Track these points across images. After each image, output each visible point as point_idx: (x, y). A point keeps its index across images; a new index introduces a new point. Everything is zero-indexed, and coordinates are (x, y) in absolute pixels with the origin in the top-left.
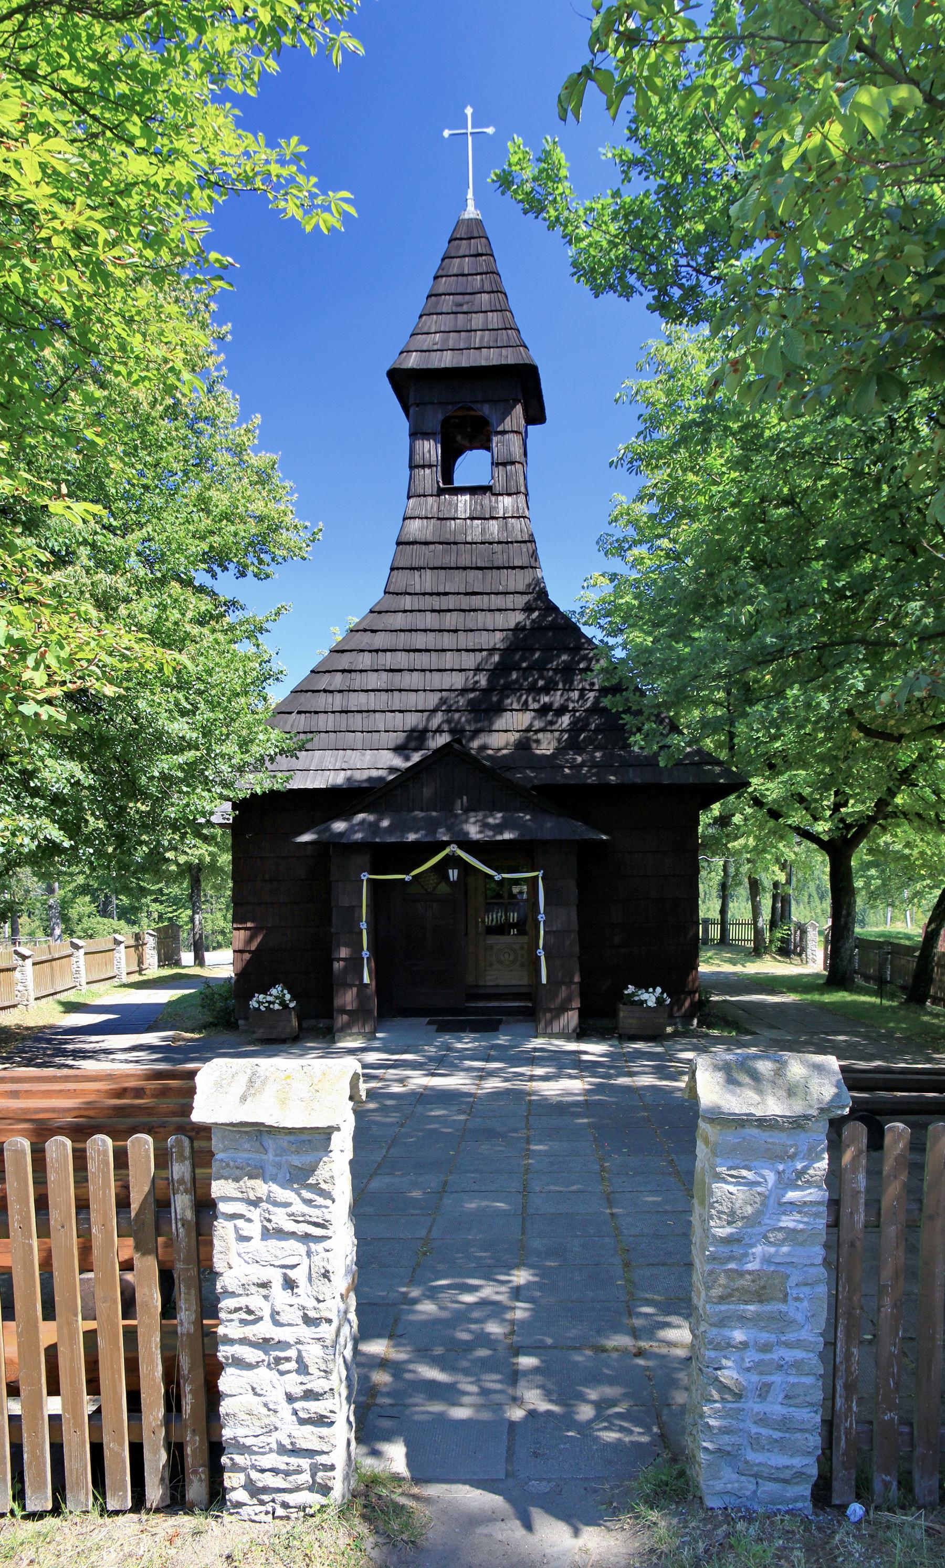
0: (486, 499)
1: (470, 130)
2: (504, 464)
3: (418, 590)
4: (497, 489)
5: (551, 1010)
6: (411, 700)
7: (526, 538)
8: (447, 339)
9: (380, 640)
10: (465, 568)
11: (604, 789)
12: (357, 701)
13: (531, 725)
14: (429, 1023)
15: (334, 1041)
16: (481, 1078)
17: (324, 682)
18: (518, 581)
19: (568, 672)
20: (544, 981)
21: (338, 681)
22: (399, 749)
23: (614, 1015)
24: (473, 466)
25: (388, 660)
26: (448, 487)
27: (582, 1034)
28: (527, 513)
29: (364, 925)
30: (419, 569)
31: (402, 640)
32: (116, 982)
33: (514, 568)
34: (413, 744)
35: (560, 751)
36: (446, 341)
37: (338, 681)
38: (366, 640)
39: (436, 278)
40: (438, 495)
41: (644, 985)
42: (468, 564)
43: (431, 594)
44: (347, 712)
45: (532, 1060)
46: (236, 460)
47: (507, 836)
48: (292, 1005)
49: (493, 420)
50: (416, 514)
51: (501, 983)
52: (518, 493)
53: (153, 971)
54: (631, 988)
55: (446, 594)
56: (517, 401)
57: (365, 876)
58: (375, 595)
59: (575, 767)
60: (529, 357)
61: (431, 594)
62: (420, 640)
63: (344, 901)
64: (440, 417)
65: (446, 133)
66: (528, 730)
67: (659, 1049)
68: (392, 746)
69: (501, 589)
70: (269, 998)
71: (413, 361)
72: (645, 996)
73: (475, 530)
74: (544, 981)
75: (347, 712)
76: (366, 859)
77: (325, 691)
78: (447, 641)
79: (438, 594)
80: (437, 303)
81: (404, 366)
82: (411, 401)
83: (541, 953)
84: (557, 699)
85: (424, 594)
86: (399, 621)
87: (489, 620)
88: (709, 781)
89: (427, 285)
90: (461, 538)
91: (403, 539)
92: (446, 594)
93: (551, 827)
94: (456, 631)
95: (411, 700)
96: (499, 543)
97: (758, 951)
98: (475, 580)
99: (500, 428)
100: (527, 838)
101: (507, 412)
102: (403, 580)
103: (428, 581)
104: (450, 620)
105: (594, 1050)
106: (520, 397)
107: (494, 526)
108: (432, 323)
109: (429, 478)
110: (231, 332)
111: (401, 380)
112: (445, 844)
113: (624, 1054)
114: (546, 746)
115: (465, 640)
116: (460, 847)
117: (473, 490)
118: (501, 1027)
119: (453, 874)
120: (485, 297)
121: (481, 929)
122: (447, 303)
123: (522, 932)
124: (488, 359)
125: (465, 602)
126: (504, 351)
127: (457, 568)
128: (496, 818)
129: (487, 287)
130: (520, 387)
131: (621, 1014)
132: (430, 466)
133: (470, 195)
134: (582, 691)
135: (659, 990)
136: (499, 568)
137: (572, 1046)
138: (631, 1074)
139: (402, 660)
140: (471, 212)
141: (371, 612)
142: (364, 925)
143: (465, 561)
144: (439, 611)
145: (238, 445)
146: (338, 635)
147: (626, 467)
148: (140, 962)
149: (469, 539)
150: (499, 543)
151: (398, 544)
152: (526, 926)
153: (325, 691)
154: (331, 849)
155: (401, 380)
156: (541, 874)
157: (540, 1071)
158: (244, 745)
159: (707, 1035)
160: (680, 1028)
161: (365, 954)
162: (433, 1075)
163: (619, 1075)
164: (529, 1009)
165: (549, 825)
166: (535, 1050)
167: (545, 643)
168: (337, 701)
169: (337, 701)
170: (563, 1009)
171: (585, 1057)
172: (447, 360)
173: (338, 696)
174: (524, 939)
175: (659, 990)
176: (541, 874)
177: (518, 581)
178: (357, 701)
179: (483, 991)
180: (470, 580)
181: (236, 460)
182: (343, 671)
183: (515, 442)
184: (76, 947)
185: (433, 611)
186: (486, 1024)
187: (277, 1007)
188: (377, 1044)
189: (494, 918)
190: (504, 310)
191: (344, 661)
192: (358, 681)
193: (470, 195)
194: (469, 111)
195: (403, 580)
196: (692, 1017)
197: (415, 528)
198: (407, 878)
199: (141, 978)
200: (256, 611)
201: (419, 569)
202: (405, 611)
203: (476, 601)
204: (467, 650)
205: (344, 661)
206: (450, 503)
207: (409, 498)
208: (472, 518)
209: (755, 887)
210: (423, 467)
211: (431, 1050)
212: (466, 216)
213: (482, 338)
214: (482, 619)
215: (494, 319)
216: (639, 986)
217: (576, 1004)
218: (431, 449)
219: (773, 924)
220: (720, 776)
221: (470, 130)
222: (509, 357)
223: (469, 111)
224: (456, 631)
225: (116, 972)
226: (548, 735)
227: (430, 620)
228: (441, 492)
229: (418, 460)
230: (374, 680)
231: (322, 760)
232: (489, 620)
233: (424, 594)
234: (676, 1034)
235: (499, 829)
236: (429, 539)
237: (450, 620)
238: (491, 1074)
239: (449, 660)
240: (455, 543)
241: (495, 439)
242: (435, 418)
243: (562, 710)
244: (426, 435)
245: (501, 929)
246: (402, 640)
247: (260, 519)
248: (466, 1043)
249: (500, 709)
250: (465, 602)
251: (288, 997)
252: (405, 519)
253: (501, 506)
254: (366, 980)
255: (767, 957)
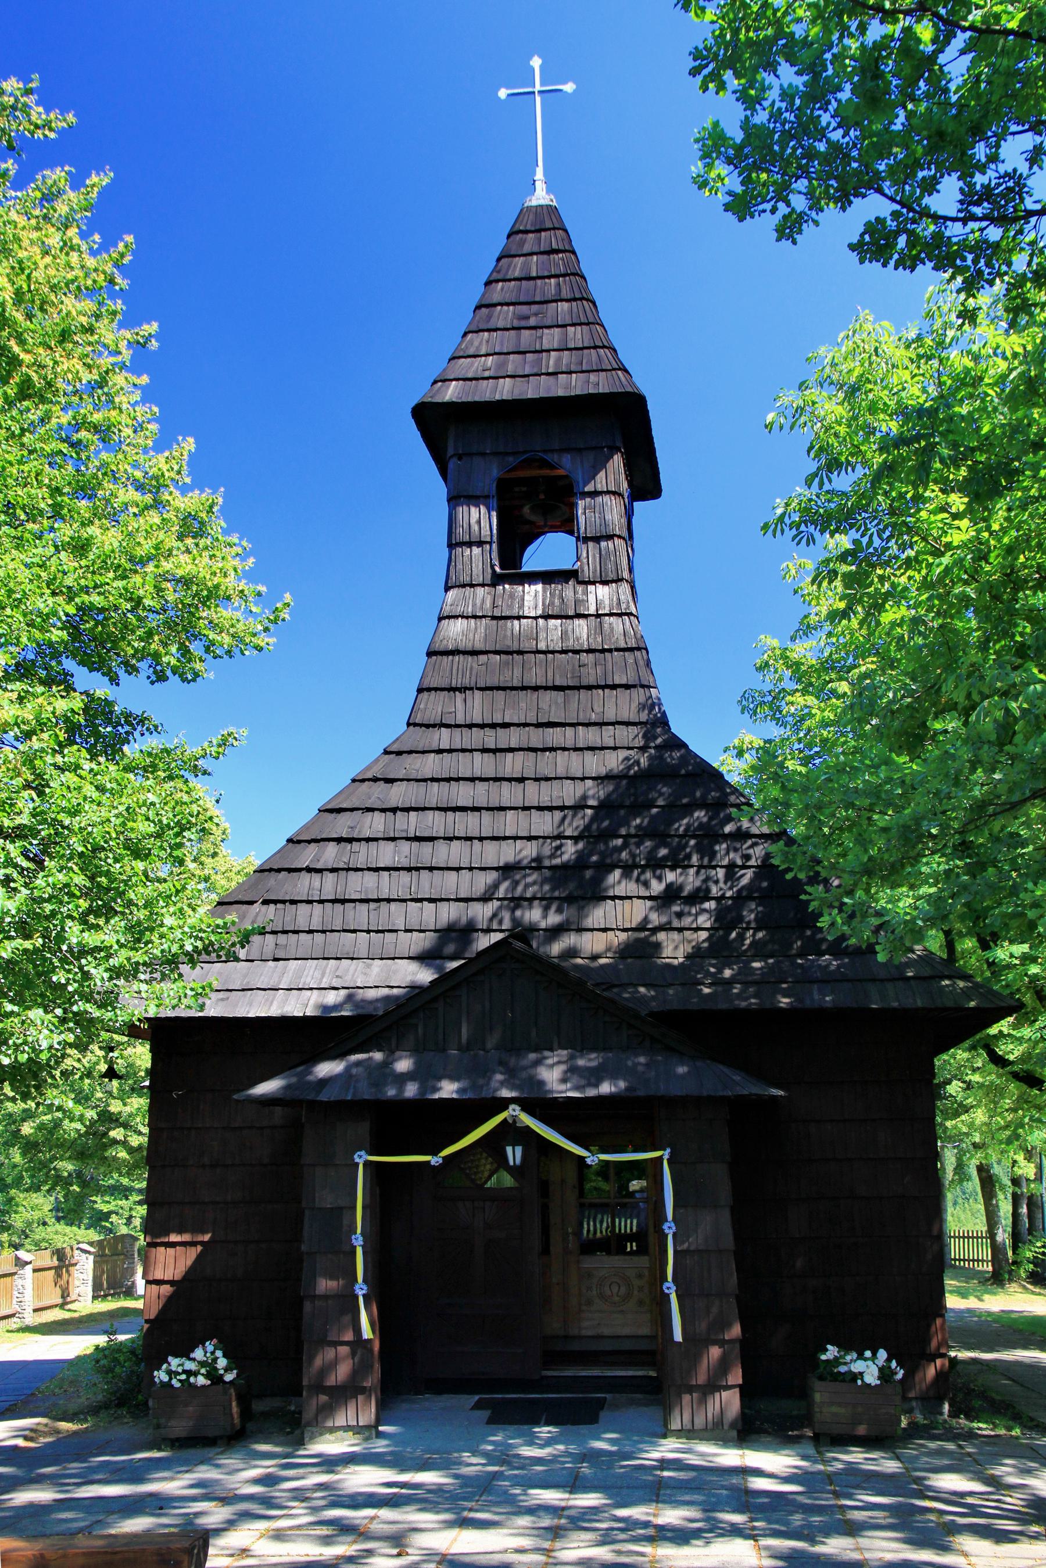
0: (569, 590)
1: (538, 87)
2: (597, 539)
3: (460, 720)
4: (586, 574)
5: (690, 1389)
6: (450, 883)
7: (632, 643)
8: (504, 364)
9: (397, 794)
10: (536, 688)
11: (770, 1017)
12: (359, 885)
13: (646, 920)
14: (478, 1406)
15: (301, 1443)
16: (555, 1533)
17: (307, 856)
18: (624, 705)
19: (708, 838)
20: (678, 1336)
21: (330, 855)
22: (424, 958)
23: (804, 1394)
24: (549, 551)
25: (412, 823)
26: (510, 570)
27: (746, 1431)
28: (634, 611)
29: (358, 1240)
30: (463, 689)
31: (435, 794)
32: (14, 1323)
33: (614, 687)
34: (450, 949)
35: (696, 955)
36: (502, 365)
37: (330, 855)
38: (376, 794)
39: (488, 284)
40: (494, 585)
41: (858, 1345)
42: (541, 682)
43: (482, 726)
44: (343, 901)
45: (656, 1488)
46: (148, 499)
47: (606, 1088)
48: (229, 1377)
49: (579, 476)
50: (459, 610)
51: (607, 1332)
52: (618, 580)
53: (85, 1304)
54: (832, 1352)
55: (506, 725)
56: (614, 449)
57: (361, 1158)
58: (393, 728)
59: (718, 982)
60: (632, 384)
61: (482, 726)
62: (463, 794)
63: (326, 1199)
64: (495, 472)
65: (503, 93)
66: (641, 927)
67: (891, 1466)
68: (414, 950)
69: (594, 718)
70: (190, 1366)
71: (451, 393)
72: (858, 1366)
73: (553, 632)
74: (678, 1336)
75: (343, 901)
76: (363, 1129)
77: (309, 870)
78: (508, 794)
79: (493, 726)
80: (489, 317)
81: (438, 399)
82: (450, 451)
83: (670, 1288)
84: (691, 880)
85: (470, 726)
86: (430, 765)
87: (574, 764)
88: (950, 1004)
89: (476, 292)
90: (526, 646)
91: (438, 646)
92: (506, 725)
93: (682, 1074)
94: (521, 780)
95: (450, 883)
96: (590, 651)
97: (998, 1278)
98: (552, 706)
99: (589, 488)
100: (641, 1093)
101: (600, 465)
102: (435, 707)
103: (477, 707)
104: (513, 764)
105: (773, 1465)
106: (619, 444)
107: (581, 629)
108: (480, 342)
109: (478, 561)
110: (157, 336)
111: (434, 421)
112: (503, 1104)
113: (829, 1478)
114: (674, 949)
115: (533, 794)
116: (523, 1109)
117: (548, 577)
118: (603, 1414)
119: (514, 1154)
120: (564, 306)
121: (572, 1244)
122: (505, 316)
123: (643, 1250)
124: (568, 386)
125: (536, 737)
126: (593, 377)
127: (524, 688)
128: (587, 1061)
129: (566, 293)
130: (620, 424)
131: (817, 1397)
132: (480, 544)
133: (539, 174)
134: (731, 868)
135: (882, 1354)
136: (589, 688)
137: (730, 1457)
138: (852, 1529)
139: (434, 823)
140: (541, 196)
141: (386, 752)
142: (358, 1240)
143: (535, 677)
144: (494, 751)
145: (156, 478)
146: (330, 785)
147: (790, 534)
148: (65, 1294)
149: (542, 646)
150: (590, 651)
151: (430, 654)
152: (648, 1241)
153: (309, 870)
154: (305, 1109)
155: (434, 421)
156: (666, 1154)
157: (671, 1516)
158: (137, 934)
159: (970, 1435)
160: (919, 1418)
161: (361, 1289)
162: (464, 1523)
163: (828, 1531)
164: (650, 1383)
165: (681, 1070)
166: (664, 1464)
167: (663, 797)
168: (329, 885)
169: (329, 885)
170: (713, 1386)
171: (759, 1484)
172: (505, 390)
173: (330, 877)
174: (643, 1261)
175: (882, 1354)
176: (666, 1154)
177: (624, 705)
178: (359, 885)
179: (576, 1346)
180: (544, 705)
181: (148, 499)
182: (339, 840)
183: (613, 511)
184: (21, 1263)
185: (484, 751)
186: (576, 1412)
187: (201, 1381)
188: (380, 1446)
189: (598, 1227)
190: (593, 322)
191: (342, 826)
192: (363, 855)
193: (539, 174)
194: (536, 62)
195: (435, 707)
196: (940, 1401)
197: (456, 631)
198: (435, 1160)
199: (67, 1315)
200: (181, 738)
201: (463, 689)
202: (440, 751)
203: (554, 736)
204: (540, 809)
205: (342, 826)
206: (512, 596)
207: (447, 589)
208: (546, 617)
209: (988, 1182)
210: (470, 544)
211: (473, 1464)
212: (534, 203)
213: (559, 360)
214: (563, 763)
215: (577, 335)
216: (845, 1346)
217: (736, 1377)
218: (480, 519)
219: (1017, 1238)
220: (966, 994)
221: (538, 87)
222: (601, 384)
223: (536, 62)
224: (521, 780)
225: (15, 1308)
226: (675, 935)
227: (482, 764)
228: (497, 580)
229: (461, 534)
230: (387, 854)
231: (299, 974)
232: (574, 764)
233: (470, 726)
234: (915, 1431)
235: (595, 1076)
236: (479, 646)
237: (513, 764)
238: (579, 1520)
239: (510, 823)
240: (520, 653)
241: (581, 504)
242: (488, 474)
243: (699, 896)
244: (473, 499)
245: (614, 1244)
246: (435, 794)
247: (186, 582)
248: (541, 1445)
249: (597, 895)
250: (536, 737)
251: (222, 1363)
252: (440, 619)
253: (592, 598)
254: (367, 1333)
255: (1013, 1287)
